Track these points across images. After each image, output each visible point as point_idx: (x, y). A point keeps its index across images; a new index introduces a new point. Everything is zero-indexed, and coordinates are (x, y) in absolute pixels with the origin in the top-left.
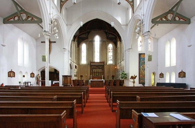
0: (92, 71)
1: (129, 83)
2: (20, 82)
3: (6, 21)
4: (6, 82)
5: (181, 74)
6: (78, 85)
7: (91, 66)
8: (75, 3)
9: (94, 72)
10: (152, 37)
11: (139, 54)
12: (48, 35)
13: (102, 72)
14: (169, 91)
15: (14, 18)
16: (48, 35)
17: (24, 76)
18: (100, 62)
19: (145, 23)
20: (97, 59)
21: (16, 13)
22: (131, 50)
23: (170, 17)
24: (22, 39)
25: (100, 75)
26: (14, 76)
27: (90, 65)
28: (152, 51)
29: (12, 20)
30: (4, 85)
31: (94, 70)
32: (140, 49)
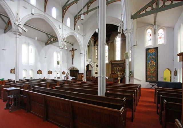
0: (113, 69)
1: (134, 81)
2: (55, 77)
3: (47, 44)
4: (7, 76)
5: (41, 72)
6: (92, 81)
7: (112, 64)
8: (83, 19)
9: (115, 70)
10: (165, 27)
11: (146, 49)
12: (61, 48)
13: (122, 70)
14: (112, 88)
15: (150, 7)
16: (61, 48)
17: (58, 74)
18: (121, 61)
19: (124, 22)
20: (118, 58)
21: (49, 40)
22: (136, 47)
23: (52, 40)
24: (57, 51)
25: (113, 72)
26: (51, 74)
27: (112, 63)
28: (166, 44)
29: (144, 12)
30: (45, 79)
31: (114, 68)
32: (149, 43)
